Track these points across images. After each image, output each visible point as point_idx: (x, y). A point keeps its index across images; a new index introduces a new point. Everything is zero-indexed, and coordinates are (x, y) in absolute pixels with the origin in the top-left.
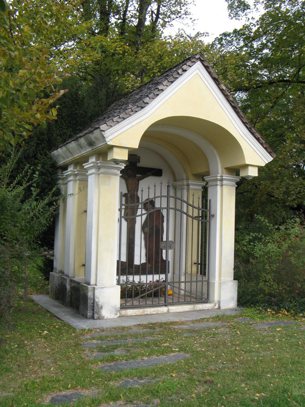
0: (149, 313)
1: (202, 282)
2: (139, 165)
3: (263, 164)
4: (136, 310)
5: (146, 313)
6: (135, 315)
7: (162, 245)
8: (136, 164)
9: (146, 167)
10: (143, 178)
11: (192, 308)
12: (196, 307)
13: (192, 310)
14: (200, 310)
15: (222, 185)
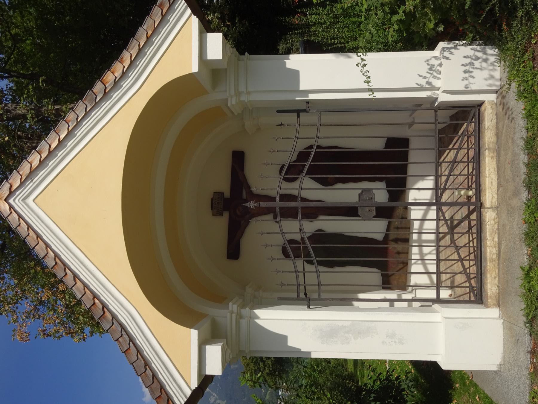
0: (495, 250)
1: (436, 120)
2: (227, 194)
3: (195, 21)
4: (488, 276)
5: (495, 256)
6: (497, 279)
8: (226, 200)
10: (249, 187)
11: (491, 155)
12: (491, 146)
13: (495, 154)
14: (498, 135)
15: (249, 93)
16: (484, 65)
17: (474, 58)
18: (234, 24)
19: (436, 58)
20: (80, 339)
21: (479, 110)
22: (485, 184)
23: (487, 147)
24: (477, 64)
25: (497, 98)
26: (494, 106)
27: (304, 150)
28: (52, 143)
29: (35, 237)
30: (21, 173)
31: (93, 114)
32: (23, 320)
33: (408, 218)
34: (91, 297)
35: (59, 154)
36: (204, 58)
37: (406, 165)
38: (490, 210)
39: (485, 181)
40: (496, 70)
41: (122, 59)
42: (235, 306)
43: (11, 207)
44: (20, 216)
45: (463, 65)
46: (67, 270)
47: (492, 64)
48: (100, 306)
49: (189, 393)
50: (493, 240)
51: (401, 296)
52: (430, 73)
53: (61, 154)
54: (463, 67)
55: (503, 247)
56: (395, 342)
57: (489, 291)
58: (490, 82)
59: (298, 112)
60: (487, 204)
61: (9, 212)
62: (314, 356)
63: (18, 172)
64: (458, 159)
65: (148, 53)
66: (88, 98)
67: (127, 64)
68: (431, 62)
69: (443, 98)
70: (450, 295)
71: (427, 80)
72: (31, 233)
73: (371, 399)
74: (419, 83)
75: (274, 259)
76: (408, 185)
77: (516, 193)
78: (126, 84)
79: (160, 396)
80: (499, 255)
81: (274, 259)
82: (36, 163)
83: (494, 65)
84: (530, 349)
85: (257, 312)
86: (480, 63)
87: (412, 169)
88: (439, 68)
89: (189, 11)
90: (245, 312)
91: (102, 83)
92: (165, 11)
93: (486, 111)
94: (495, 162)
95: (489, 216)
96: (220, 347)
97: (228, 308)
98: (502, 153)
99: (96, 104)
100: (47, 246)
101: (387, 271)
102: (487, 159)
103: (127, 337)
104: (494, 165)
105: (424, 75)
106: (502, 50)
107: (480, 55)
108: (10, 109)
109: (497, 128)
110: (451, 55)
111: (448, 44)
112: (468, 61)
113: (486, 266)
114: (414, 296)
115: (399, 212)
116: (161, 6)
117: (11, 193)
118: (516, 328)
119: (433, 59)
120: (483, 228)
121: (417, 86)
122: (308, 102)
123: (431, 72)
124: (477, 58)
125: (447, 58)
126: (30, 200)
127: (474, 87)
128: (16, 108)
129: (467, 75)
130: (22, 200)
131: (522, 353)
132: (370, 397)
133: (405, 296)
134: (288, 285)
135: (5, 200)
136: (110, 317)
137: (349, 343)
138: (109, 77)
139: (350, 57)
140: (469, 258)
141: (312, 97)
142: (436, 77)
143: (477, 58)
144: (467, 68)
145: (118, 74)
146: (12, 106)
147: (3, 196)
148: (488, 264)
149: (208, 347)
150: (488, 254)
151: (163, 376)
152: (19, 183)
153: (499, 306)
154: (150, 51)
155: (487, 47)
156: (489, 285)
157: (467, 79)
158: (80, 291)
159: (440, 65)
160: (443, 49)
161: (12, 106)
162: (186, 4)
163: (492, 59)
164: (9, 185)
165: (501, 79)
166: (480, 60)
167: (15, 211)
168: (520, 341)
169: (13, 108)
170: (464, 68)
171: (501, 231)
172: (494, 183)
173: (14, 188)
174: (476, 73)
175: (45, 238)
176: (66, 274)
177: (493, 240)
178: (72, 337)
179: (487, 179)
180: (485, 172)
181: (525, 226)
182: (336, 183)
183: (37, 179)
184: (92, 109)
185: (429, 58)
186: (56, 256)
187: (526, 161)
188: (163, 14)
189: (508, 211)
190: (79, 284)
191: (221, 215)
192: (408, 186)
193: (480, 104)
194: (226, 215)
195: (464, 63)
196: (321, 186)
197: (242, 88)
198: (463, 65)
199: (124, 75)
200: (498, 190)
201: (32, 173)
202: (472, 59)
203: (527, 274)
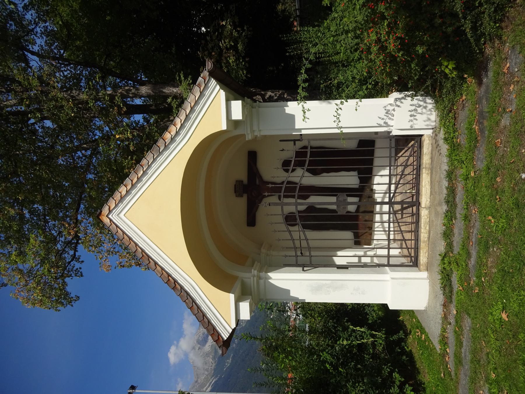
0: (426, 235)
2: (245, 181)
3: (222, 93)
4: (421, 251)
5: (426, 239)
7: (341, 212)
9: (246, 204)
10: (260, 177)
11: (427, 172)
12: (427, 166)
13: (430, 171)
14: (432, 158)
16: (424, 110)
17: (417, 106)
18: (243, 30)
19: (390, 104)
20: (146, 269)
21: (421, 139)
22: (422, 191)
23: (424, 167)
24: (419, 110)
25: (433, 133)
26: (430, 138)
27: (300, 150)
28: (133, 179)
29: (128, 240)
30: (115, 199)
31: (158, 159)
32: (106, 256)
33: (373, 197)
34: (167, 276)
35: (138, 186)
36: (230, 119)
37: (373, 159)
38: (424, 209)
39: (422, 189)
40: (432, 114)
41: (175, 123)
42: (256, 272)
43: (111, 220)
44: (117, 226)
45: (410, 111)
46: (150, 260)
47: (430, 110)
48: (173, 281)
49: (230, 331)
50: (425, 229)
51: (366, 253)
52: (387, 116)
53: (139, 185)
54: (410, 112)
55: (431, 235)
56: (359, 293)
57: (421, 261)
58: (428, 123)
59: (295, 141)
60: (423, 204)
61: (110, 224)
62: (306, 301)
63: (113, 198)
64: (409, 163)
65: (192, 118)
66: (155, 150)
67: (179, 126)
68: (387, 108)
69: (395, 133)
70: (400, 253)
71: (384, 121)
72: (125, 237)
73: (345, 321)
74: (379, 123)
75: (280, 240)
76: (374, 173)
77: (440, 204)
78: (178, 139)
79: (213, 334)
80: (429, 238)
81: (280, 240)
82: (124, 193)
83: (431, 111)
84: (443, 303)
85: (270, 274)
86: (422, 109)
87: (377, 162)
88: (393, 112)
89: (218, 87)
90: (262, 274)
91: (163, 139)
92: (202, 89)
93: (425, 142)
94: (429, 177)
95: (424, 213)
96: (248, 304)
97: (251, 272)
98: (434, 173)
99: (160, 153)
100: (136, 245)
101: (357, 230)
102: (424, 175)
103: (190, 300)
104: (429, 179)
105: (382, 117)
106: (436, 102)
107: (421, 103)
108: (75, 95)
109: (432, 153)
110: (401, 104)
111: (400, 94)
112: (413, 108)
113: (420, 245)
114: (375, 253)
115: (367, 192)
116: (199, 86)
117: (110, 212)
118: (436, 288)
119: (389, 106)
120: (420, 219)
121: (377, 125)
122: (301, 135)
123: (388, 115)
124: (420, 106)
125: (399, 106)
126: (122, 215)
127: (416, 127)
128: (79, 94)
129: (412, 118)
130: (117, 215)
131: (438, 304)
132: (344, 320)
133: (369, 253)
134: (290, 256)
135: (107, 216)
136: (179, 288)
137: (329, 294)
138: (167, 136)
139: (330, 103)
140: (409, 240)
141: (304, 132)
142: (391, 118)
143: (420, 106)
144: (412, 113)
145: (173, 133)
146: (76, 93)
147: (105, 214)
148: (422, 244)
149: (241, 303)
150: (422, 238)
151: (214, 322)
152: (114, 205)
153: (427, 271)
154: (193, 116)
155: (427, 98)
156: (421, 257)
157: (412, 121)
158: (159, 273)
159: (394, 110)
160: (396, 100)
161: (76, 93)
162: (216, 83)
163: (430, 106)
164: (108, 207)
165: (435, 121)
166: (421, 108)
167: (113, 223)
168: (438, 296)
169: (77, 94)
170: (410, 113)
171: (431, 223)
172: (428, 191)
173: (111, 208)
174: (418, 116)
175: (134, 239)
176: (150, 262)
177: (425, 229)
178: (140, 267)
179: (423, 188)
180: (422, 183)
181: (444, 227)
182: (322, 173)
183: (125, 202)
184: (157, 157)
185: (386, 105)
186: (143, 251)
187: (447, 185)
188: (201, 91)
189: (435, 213)
190: (158, 267)
191: (242, 196)
192: (374, 173)
193: (421, 136)
194: (245, 196)
195: (410, 110)
196: (312, 175)
197: (255, 128)
198: (410, 111)
199: (177, 133)
200: (430, 196)
201: (122, 198)
202: (416, 106)
203: (443, 259)
